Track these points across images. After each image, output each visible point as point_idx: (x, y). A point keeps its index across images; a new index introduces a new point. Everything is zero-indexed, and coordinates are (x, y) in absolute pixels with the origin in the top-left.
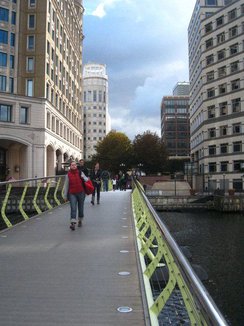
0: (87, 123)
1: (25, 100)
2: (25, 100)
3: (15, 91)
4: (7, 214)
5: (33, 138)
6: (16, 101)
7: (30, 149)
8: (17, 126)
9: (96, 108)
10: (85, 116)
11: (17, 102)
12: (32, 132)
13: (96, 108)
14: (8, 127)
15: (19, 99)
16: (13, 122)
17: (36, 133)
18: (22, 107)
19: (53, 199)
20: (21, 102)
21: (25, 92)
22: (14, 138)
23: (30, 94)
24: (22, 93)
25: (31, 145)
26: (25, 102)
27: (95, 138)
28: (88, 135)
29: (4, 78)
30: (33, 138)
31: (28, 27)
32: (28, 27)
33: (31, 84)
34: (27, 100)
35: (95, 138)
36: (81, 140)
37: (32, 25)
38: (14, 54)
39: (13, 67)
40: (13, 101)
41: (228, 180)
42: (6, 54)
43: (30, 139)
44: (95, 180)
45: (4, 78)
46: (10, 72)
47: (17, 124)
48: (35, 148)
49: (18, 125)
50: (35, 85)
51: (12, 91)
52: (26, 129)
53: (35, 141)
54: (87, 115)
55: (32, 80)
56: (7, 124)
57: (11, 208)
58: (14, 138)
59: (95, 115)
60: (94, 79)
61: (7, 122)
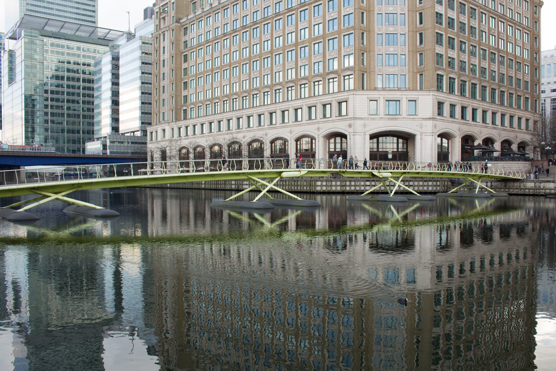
5: (421, 128)
6: (403, 96)
7: (418, 138)
11: (404, 97)
14: (396, 119)
20: (408, 96)
25: (419, 134)
48: (423, 137)
61: (396, 115)
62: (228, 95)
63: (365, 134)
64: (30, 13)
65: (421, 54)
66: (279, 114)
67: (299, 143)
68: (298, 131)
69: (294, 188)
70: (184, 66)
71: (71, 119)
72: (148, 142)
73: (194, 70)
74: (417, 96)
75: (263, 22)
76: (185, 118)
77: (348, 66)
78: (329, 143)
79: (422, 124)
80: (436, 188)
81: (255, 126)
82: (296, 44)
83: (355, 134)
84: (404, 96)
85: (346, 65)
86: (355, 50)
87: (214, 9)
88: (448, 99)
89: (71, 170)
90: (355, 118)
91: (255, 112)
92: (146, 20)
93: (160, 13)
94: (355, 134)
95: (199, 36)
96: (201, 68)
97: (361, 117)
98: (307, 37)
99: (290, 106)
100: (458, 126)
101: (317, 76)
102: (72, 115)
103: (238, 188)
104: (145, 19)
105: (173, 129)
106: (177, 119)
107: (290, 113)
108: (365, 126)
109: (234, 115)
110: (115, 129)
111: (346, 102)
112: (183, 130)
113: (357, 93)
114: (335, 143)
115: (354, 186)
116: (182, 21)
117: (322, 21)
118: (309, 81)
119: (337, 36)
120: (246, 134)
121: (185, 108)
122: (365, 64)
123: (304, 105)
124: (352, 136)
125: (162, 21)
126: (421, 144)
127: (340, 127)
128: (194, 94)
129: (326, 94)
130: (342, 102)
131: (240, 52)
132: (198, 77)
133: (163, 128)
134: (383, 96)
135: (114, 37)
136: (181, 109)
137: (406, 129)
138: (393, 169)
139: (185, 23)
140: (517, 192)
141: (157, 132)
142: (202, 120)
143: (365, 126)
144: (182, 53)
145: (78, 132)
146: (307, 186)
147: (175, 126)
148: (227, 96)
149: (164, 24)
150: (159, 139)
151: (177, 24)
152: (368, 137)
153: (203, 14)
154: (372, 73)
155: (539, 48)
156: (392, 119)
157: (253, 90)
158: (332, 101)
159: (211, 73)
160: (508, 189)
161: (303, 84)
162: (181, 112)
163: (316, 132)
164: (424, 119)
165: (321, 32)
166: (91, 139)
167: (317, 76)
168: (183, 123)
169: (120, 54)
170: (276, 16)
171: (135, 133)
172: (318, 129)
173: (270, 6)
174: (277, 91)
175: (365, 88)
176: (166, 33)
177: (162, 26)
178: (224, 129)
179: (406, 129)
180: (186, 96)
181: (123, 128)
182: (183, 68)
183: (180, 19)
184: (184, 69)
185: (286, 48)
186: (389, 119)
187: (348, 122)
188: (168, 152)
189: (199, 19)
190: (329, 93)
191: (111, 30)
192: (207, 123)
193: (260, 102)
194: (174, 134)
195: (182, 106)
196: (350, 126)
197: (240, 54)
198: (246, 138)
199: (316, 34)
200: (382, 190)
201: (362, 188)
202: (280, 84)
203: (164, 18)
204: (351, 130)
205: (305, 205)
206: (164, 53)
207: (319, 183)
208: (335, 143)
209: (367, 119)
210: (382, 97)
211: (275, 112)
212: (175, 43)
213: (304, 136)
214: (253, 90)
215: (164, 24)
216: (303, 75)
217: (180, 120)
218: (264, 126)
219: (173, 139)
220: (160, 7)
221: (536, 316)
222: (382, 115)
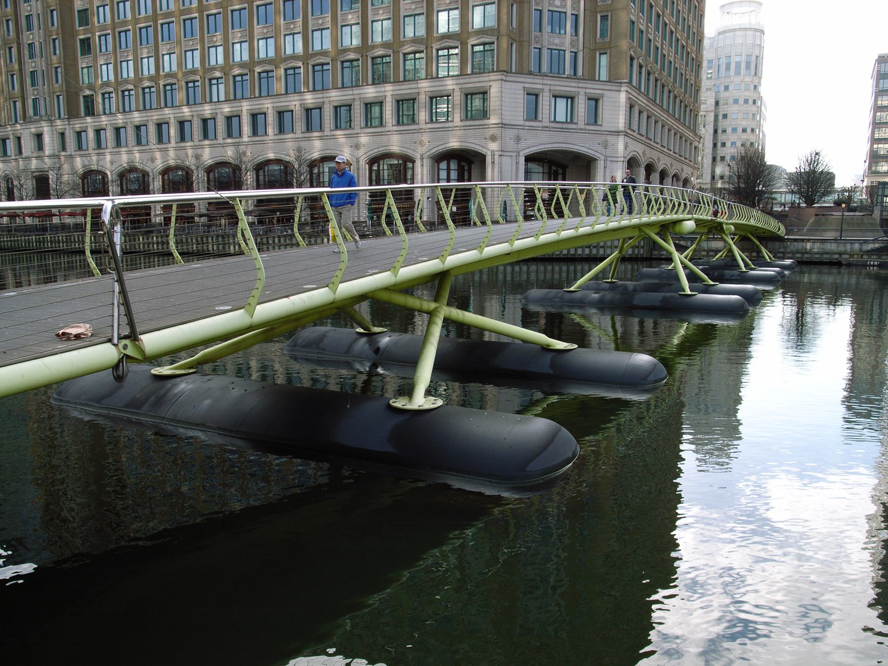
1: (593, 86)
2: (593, 86)
3: (580, 73)
4: (92, 252)
6: (580, 90)
7: (600, 164)
8: (581, 129)
9: (734, 100)
10: (717, 103)
11: (582, 91)
12: (604, 137)
13: (734, 100)
15: (585, 85)
16: (575, 124)
17: (610, 139)
18: (589, 99)
20: (588, 91)
21: (595, 73)
22: (576, 147)
23: (604, 76)
24: (591, 76)
25: (602, 158)
26: (593, 89)
27: (733, 144)
28: (721, 137)
29: (563, 15)
30: (606, 147)
33: (604, 59)
34: (597, 87)
35: (733, 144)
38: (579, 11)
39: (577, 34)
40: (576, 90)
42: (565, 13)
43: (600, 149)
44: (698, 222)
45: (563, 15)
46: (572, 41)
47: (581, 125)
48: (608, 163)
49: (583, 127)
50: (610, 62)
51: (575, 74)
52: (596, 133)
53: (609, 152)
54: (721, 103)
55: (606, 53)
56: (565, 126)
61: (566, 122)
63: (518, 156)
65: (604, 18)
74: (600, 92)
77: (412, 35)
78: (439, 169)
79: (607, 141)
80: (598, 252)
83: (503, 153)
85: (289, 51)
88: (642, 101)
94: (503, 153)
97: (513, 123)
99: (357, 97)
106: (72, 114)
108: (518, 139)
109: (246, 107)
111: (320, 109)
114: (448, 170)
118: (461, 44)
122: (514, 25)
129: (255, 97)
130: (283, 112)
134: (548, 87)
138: (663, 213)
140: (807, 258)
141: (19, 139)
143: (518, 139)
152: (522, 160)
154: (525, 44)
155: (703, 33)
159: (110, 31)
161: (191, 82)
178: (13, 152)
179: (583, 149)
185: (159, 17)
188: (52, 176)
190: (437, 77)
198: (523, 144)
200: (564, 255)
201: (601, 252)
209: (523, 127)
210: (547, 88)
216: (167, 69)
218: (87, 150)
221: (682, 447)
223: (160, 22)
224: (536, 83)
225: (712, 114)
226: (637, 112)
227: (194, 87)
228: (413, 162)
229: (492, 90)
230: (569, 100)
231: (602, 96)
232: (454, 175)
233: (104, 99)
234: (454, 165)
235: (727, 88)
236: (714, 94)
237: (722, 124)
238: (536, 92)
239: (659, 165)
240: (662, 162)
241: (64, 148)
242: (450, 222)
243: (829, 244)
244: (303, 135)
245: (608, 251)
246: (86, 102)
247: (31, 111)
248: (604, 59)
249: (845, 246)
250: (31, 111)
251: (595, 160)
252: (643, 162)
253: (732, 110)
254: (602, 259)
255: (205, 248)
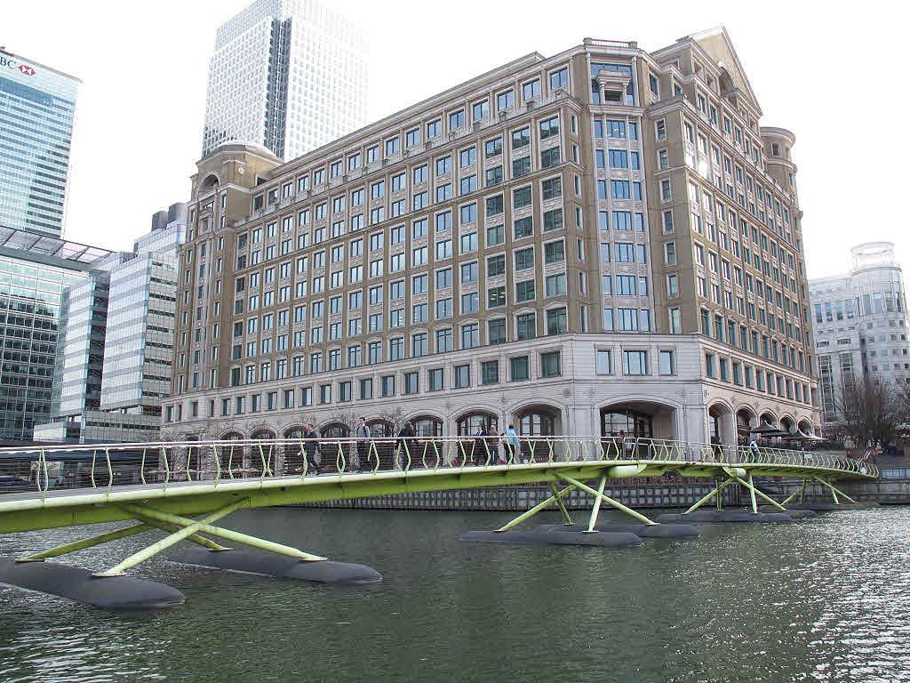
0: (868, 354)
5: (683, 396)
7: (680, 413)
10: (863, 341)
11: (617, 345)
14: (642, 382)
19: (346, 463)
23: (678, 329)
25: (564, 407)
26: (666, 342)
30: (683, 396)
31: (664, 230)
32: (664, 230)
33: (677, 313)
36: (813, 390)
37: (669, 226)
41: (712, 438)
43: (679, 398)
54: (867, 340)
56: (639, 378)
57: (587, 503)
58: (660, 400)
59: (883, 339)
60: (873, 272)
62: (321, 344)
64: (66, 106)
66: (317, 389)
67: (463, 425)
68: (463, 403)
69: (419, 503)
70: (238, 296)
71: (36, 389)
72: (163, 423)
73: (255, 304)
75: (391, 225)
76: (236, 383)
81: (315, 404)
82: (407, 273)
84: (654, 344)
86: (568, 267)
87: (412, 161)
88: (723, 350)
89: (41, 478)
90: (575, 381)
91: (375, 372)
92: (155, 232)
93: (199, 212)
95: (268, 248)
96: (271, 300)
98: (341, 284)
100: (731, 394)
101: (443, 321)
102: (12, 378)
103: (354, 505)
104: (153, 229)
105: (213, 402)
106: (222, 385)
107: (375, 385)
109: (334, 378)
110: (92, 403)
112: (232, 404)
113: (578, 338)
114: (531, 424)
115: (585, 498)
116: (236, 225)
117: (382, 257)
119: (477, 259)
120: (402, 405)
121: (236, 367)
123: (422, 367)
124: (571, 411)
125: (201, 225)
126: (685, 421)
127: (547, 394)
128: (255, 345)
131: (327, 279)
132: (262, 313)
133: (194, 400)
135: (92, 258)
136: (228, 368)
137: (608, 401)
139: (243, 228)
141: (180, 406)
142: (270, 387)
143: (592, 393)
144: (236, 276)
145: (20, 407)
146: (499, 500)
147: (217, 396)
148: (318, 346)
149: (206, 228)
150: (185, 418)
151: (228, 229)
152: (597, 413)
153: (478, 136)
154: (597, 307)
156: (636, 382)
157: (371, 335)
158: (530, 352)
160: (644, 488)
162: (229, 372)
163: (500, 405)
164: (689, 382)
165: (381, 273)
166: (46, 420)
167: (443, 321)
168: (232, 392)
169: (112, 280)
170: (416, 216)
171: (128, 410)
172: (503, 400)
173: (474, 175)
174: (353, 350)
175: (586, 330)
176: (208, 243)
177: (201, 232)
180: (240, 346)
181: (106, 400)
182: (235, 300)
183: (234, 222)
184: (545, 214)
186: (632, 382)
187: (562, 388)
189: (268, 222)
191: (89, 247)
192: (280, 392)
193: (384, 355)
194: (215, 410)
195: (232, 363)
196: (567, 393)
197: (276, 297)
198: (454, 408)
199: (374, 274)
201: (682, 500)
202: (301, 350)
203: (205, 220)
204: (568, 400)
205: (595, 549)
206: (201, 275)
207: (523, 495)
208: (531, 424)
210: (617, 345)
211: (330, 385)
212: (223, 258)
213: (473, 414)
214: (371, 335)
215: (206, 228)
217: (226, 386)
219: (212, 418)
220: (198, 203)
222: (619, 376)
223: (460, 264)
224: (605, 341)
225: (859, 352)
226: (717, 364)
227: (336, 355)
228: (496, 418)
229: (564, 349)
230: (643, 354)
231: (675, 348)
232: (537, 429)
233: (248, 371)
234: (537, 419)
235: (870, 326)
236: (857, 333)
237: (871, 362)
238: (608, 348)
239: (758, 411)
240: (761, 407)
241: (212, 415)
242: (232, 477)
243: (857, 486)
244: (402, 397)
245: (690, 500)
246: (234, 375)
247: (191, 385)
248: (677, 313)
249: (900, 486)
250: (191, 385)
251: (673, 409)
252: (734, 408)
253: (878, 347)
254: (700, 507)
255: (390, 504)
